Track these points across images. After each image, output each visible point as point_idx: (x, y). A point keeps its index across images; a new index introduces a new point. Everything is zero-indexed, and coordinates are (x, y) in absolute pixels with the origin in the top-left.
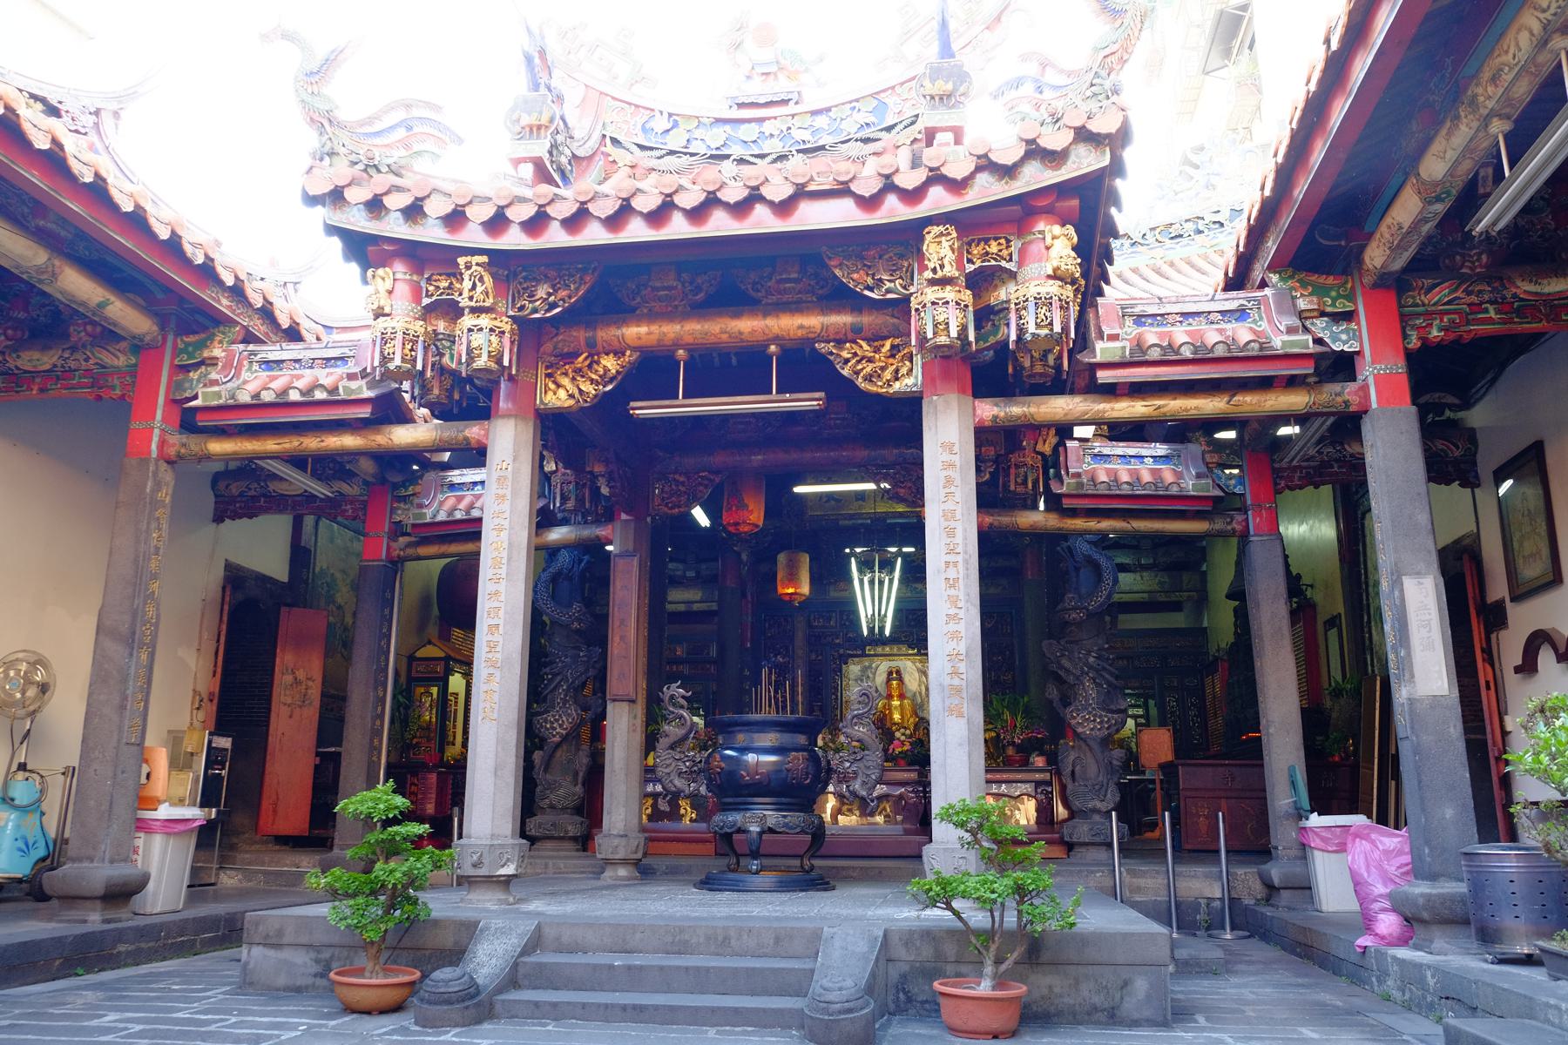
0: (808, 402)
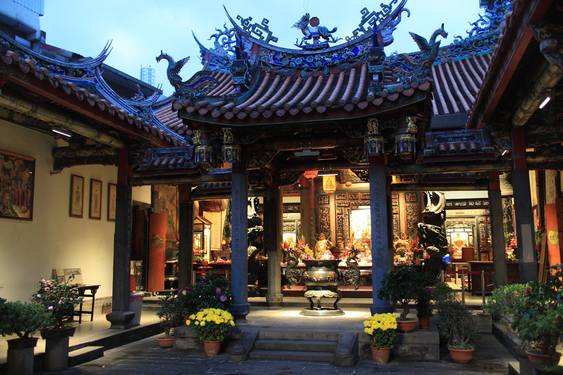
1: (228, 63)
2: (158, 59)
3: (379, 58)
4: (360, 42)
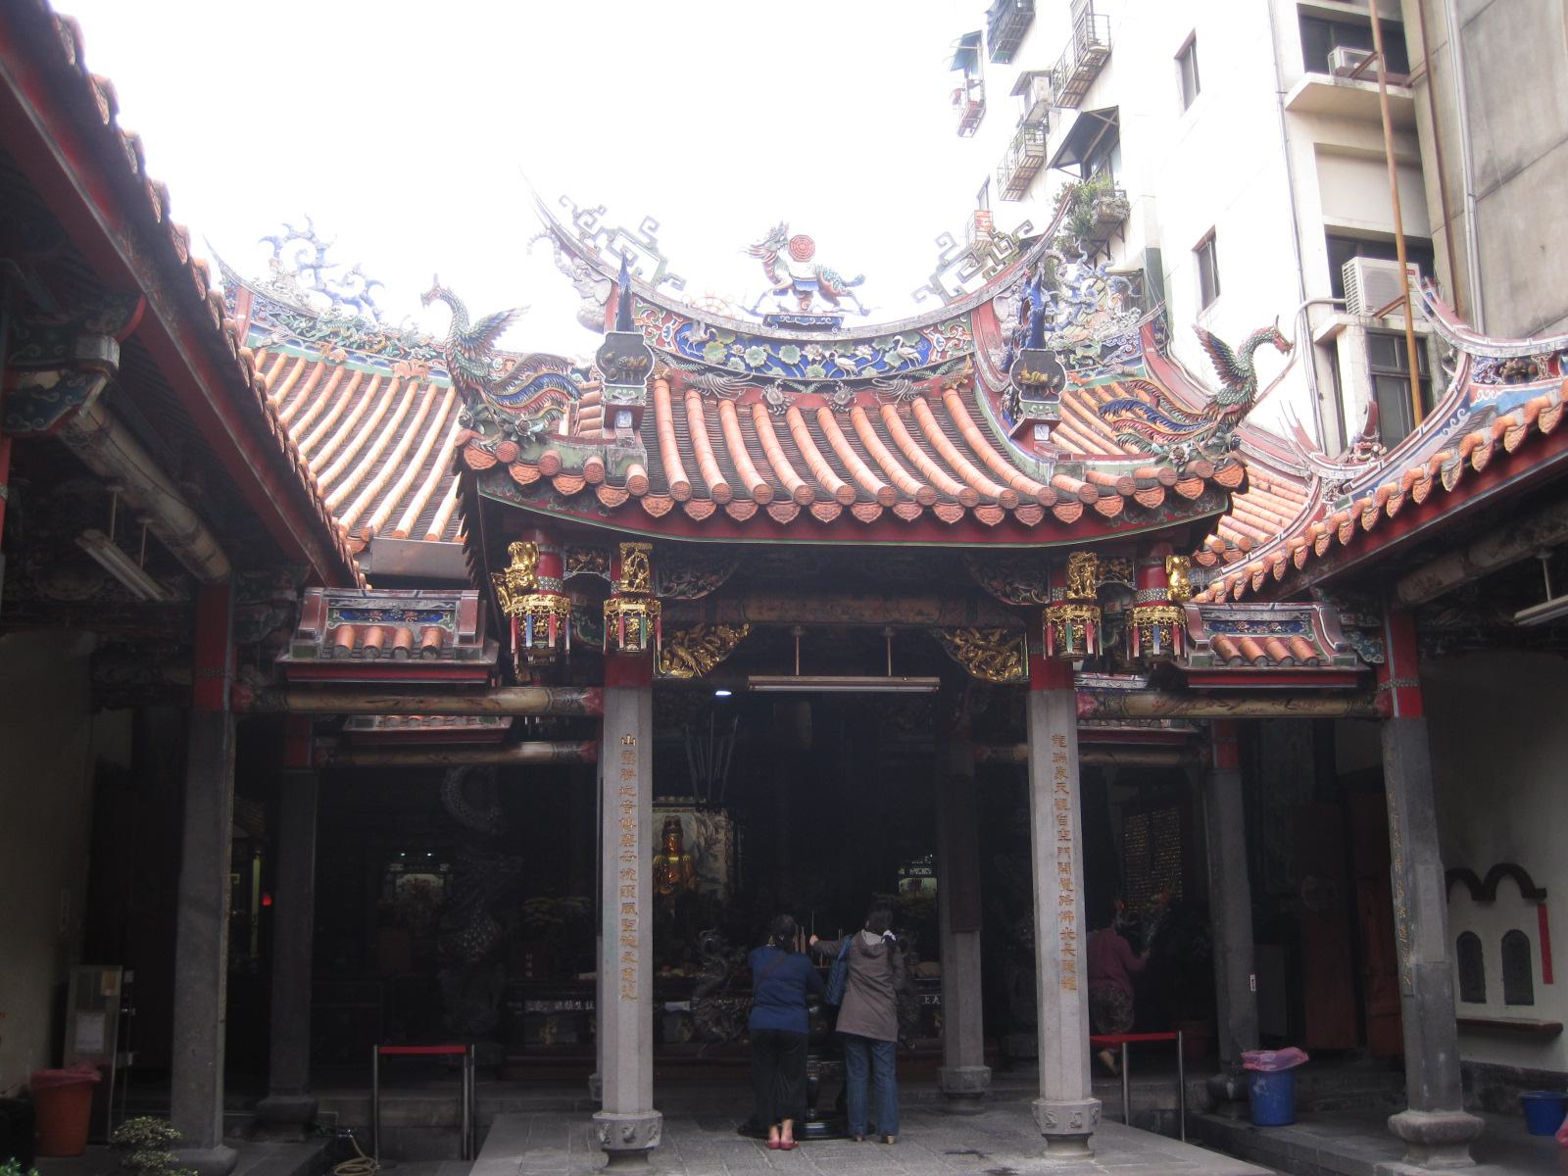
0: (925, 684)
1: (312, 328)
2: (427, 299)
3: (1050, 379)
4: (935, 325)
